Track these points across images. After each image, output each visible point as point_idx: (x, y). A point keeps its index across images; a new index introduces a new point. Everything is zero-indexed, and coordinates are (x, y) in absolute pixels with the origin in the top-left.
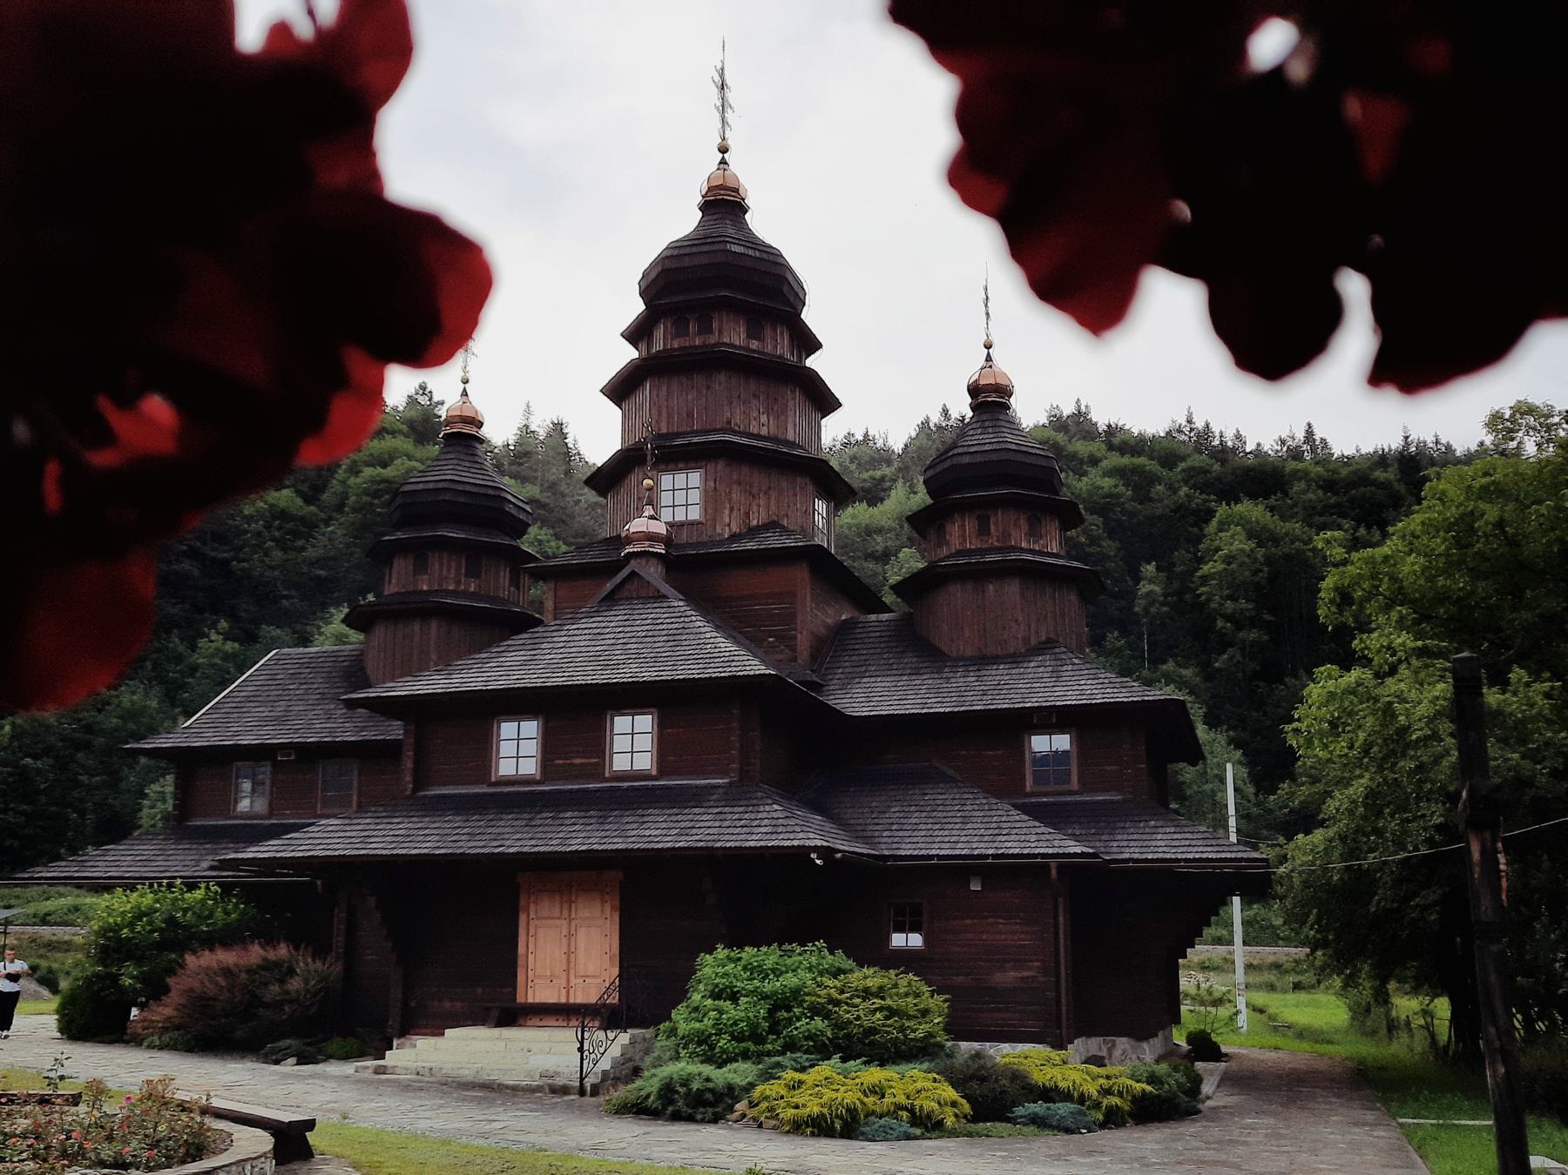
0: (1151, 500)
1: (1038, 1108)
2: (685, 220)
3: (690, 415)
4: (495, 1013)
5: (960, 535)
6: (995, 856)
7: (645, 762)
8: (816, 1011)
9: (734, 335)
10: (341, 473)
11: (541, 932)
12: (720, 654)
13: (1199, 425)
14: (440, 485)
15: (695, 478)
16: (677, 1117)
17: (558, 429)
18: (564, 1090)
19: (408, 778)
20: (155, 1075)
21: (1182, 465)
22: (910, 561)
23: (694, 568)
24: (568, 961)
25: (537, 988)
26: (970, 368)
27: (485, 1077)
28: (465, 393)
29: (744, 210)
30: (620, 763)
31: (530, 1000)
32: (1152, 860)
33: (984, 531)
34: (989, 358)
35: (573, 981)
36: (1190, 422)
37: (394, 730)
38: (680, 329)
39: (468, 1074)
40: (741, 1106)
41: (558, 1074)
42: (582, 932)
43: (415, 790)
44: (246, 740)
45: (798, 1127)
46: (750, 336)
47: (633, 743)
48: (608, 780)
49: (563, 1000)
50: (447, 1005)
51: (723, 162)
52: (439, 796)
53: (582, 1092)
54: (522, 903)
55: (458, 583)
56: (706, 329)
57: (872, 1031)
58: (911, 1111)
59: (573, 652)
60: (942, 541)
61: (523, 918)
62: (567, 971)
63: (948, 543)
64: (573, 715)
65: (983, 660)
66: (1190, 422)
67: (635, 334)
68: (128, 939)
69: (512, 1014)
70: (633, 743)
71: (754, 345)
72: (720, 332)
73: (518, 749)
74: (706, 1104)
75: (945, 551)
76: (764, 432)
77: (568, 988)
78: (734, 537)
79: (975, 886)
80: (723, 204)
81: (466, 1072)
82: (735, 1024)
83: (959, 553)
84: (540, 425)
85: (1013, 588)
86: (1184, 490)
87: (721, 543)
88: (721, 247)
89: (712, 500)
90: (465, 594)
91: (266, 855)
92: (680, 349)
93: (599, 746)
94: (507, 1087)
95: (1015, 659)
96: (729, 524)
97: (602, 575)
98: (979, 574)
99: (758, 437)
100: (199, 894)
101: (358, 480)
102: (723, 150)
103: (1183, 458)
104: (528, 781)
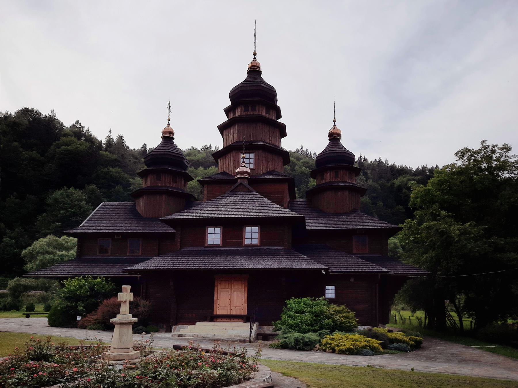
0: (295, 170)
1: (395, 345)
2: (242, 76)
3: (250, 136)
4: (209, 318)
5: (329, 178)
6: (361, 272)
7: (256, 241)
8: (328, 317)
9: (262, 112)
10: (53, 147)
11: (222, 293)
12: (275, 210)
13: (305, 150)
14: (166, 153)
15: (252, 155)
16: (300, 349)
17: (121, 138)
18: (244, 341)
19: (179, 245)
20: (98, 338)
21: (301, 161)
22: (313, 183)
23: (256, 183)
24: (231, 302)
25: (220, 309)
26: (329, 128)
27: (216, 337)
28: (169, 124)
29: (260, 73)
30: (247, 241)
31: (218, 314)
32: (367, 272)
33: (336, 176)
34: (335, 125)
35: (232, 308)
36: (302, 148)
37: (171, 230)
38: (246, 110)
39: (210, 336)
40: (317, 346)
41: (240, 336)
42: (235, 293)
43: (180, 248)
44: (106, 231)
45: (343, 352)
46: (266, 113)
47: (252, 235)
48: (243, 247)
49: (229, 314)
50: (190, 315)
51: (255, 58)
52: (189, 250)
53: (250, 342)
54: (216, 284)
55: (170, 184)
56: (254, 110)
57: (342, 323)
58: (370, 346)
59: (230, 207)
60: (323, 178)
61: (216, 289)
62: (230, 305)
63: (325, 179)
64: (233, 227)
65: (338, 214)
66: (302, 148)
67: (227, 111)
68: (79, 295)
69: (213, 318)
70: (252, 235)
71: (268, 116)
72: (259, 111)
73: (214, 236)
74: (308, 345)
75: (324, 182)
76: (270, 143)
77: (230, 310)
78: (264, 174)
79: (352, 280)
80: (254, 71)
81: (209, 336)
82: (307, 321)
83: (329, 182)
84: (114, 137)
85: (346, 193)
86: (303, 168)
87: (261, 176)
88: (259, 84)
89: (257, 162)
90: (172, 187)
91: (142, 268)
92: (246, 115)
93: (241, 236)
94: (225, 340)
95: (347, 214)
96: (262, 170)
97: (226, 185)
98: (336, 189)
99: (269, 144)
100: (99, 280)
101: (60, 150)
102: (255, 54)
103: (301, 159)
104: (217, 246)
